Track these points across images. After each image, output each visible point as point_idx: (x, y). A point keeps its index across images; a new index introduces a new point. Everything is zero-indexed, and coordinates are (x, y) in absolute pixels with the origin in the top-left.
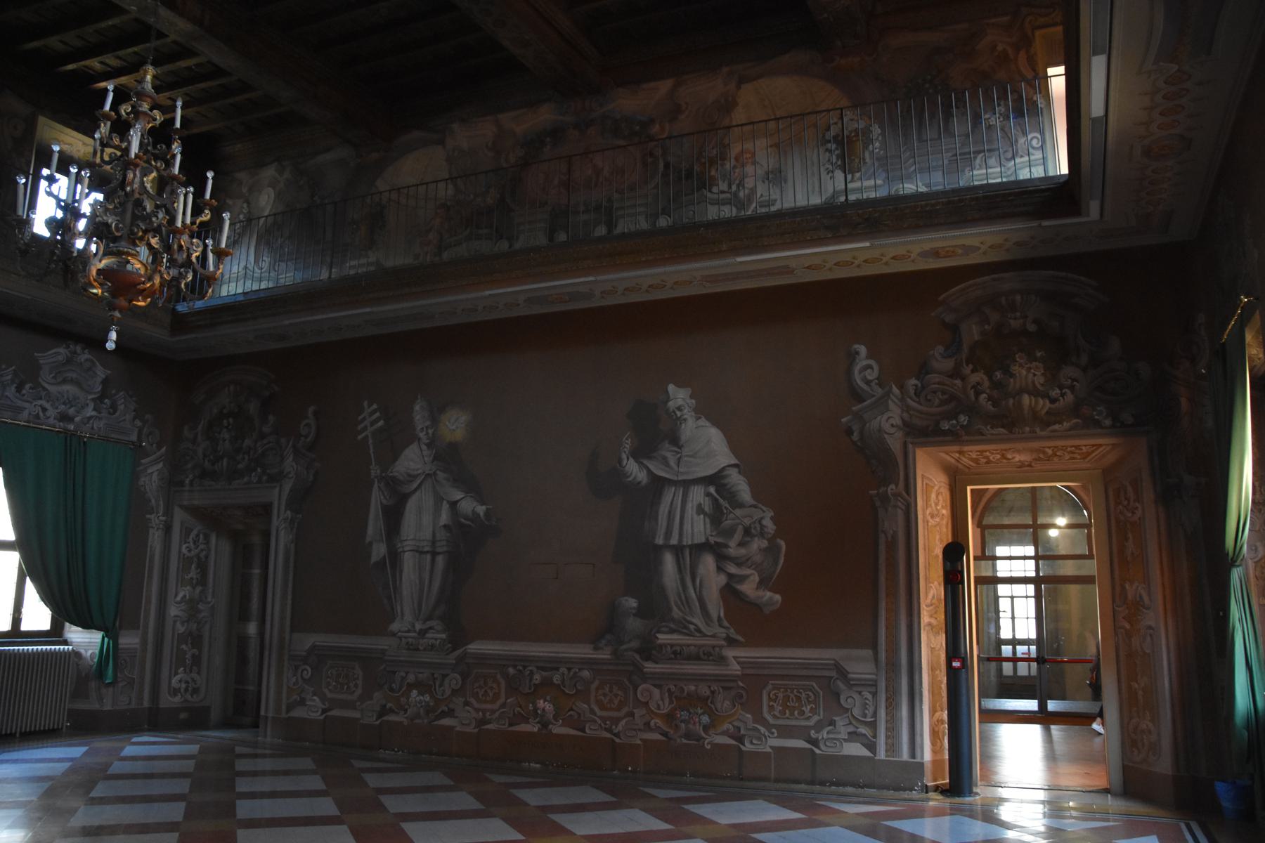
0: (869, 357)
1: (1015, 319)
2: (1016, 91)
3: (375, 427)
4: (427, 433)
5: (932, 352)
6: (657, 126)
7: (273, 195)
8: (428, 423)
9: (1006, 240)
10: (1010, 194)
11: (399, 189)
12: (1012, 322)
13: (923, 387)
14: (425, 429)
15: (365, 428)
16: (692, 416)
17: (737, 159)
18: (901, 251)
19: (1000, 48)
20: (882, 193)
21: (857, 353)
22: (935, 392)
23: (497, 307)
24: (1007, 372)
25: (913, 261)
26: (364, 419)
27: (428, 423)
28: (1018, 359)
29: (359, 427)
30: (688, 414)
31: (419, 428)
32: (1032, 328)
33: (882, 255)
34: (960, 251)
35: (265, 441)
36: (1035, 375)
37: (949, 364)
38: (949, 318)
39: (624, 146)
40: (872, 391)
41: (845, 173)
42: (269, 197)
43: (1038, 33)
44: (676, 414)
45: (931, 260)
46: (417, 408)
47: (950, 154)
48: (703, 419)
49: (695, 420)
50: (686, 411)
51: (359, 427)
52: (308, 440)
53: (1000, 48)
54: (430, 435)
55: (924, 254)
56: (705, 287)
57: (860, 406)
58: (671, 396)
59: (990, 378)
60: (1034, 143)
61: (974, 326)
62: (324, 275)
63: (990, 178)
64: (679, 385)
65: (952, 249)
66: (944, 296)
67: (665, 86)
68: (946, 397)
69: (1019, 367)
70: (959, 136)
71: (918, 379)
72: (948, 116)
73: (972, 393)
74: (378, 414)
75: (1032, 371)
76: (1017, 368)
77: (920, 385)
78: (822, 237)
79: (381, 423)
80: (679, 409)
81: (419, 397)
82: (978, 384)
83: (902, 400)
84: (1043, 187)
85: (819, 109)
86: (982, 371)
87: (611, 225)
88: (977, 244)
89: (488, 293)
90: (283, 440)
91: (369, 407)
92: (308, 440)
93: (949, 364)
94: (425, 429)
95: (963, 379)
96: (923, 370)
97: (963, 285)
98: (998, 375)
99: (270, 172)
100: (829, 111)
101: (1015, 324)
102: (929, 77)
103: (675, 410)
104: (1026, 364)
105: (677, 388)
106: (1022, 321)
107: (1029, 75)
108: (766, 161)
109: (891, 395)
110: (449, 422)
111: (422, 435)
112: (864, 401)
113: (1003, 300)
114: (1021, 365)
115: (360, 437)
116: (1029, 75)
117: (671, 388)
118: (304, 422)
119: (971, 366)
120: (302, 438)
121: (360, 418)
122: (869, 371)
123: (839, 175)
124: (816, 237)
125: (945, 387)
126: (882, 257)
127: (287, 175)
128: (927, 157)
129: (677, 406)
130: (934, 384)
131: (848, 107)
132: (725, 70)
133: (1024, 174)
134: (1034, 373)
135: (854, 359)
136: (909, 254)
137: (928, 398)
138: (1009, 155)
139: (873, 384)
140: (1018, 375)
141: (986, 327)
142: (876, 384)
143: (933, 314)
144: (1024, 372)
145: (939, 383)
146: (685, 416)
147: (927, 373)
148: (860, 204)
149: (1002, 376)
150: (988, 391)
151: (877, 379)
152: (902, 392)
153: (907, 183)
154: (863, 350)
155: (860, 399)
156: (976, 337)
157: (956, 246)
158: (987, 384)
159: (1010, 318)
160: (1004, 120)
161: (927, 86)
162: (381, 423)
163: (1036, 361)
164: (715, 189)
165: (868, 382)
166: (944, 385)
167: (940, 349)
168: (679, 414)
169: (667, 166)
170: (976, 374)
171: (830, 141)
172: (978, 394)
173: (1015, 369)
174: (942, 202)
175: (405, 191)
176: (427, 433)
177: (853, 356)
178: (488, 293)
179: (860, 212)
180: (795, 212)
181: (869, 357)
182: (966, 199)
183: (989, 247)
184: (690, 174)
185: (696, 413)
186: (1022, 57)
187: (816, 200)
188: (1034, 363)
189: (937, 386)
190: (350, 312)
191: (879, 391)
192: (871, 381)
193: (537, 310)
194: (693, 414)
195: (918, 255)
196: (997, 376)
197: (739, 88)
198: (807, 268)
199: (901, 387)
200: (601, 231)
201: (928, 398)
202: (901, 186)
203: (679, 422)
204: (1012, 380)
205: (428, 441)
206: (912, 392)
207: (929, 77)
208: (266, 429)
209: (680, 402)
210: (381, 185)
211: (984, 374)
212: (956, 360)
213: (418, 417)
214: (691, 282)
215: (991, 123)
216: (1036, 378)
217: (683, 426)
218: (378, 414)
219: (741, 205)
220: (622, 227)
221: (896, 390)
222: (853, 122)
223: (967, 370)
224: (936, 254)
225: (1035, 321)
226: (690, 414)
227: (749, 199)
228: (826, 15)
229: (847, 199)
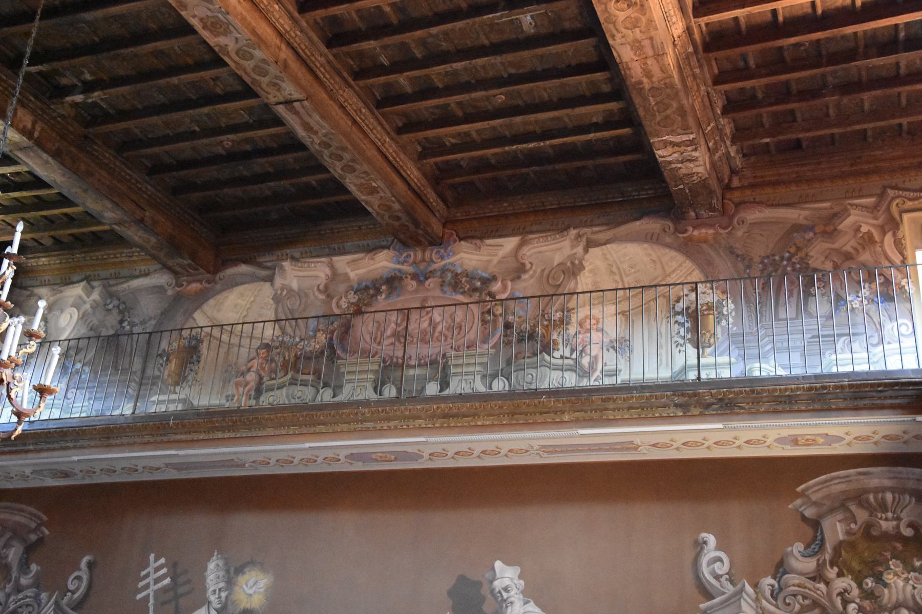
0: (718, 548)
1: (886, 519)
2: (883, 275)
3: (160, 585)
4: (220, 597)
5: (789, 549)
6: (500, 283)
7: (75, 317)
8: (222, 585)
9: (904, 432)
10: (879, 385)
11: (223, 325)
12: (882, 522)
13: (781, 589)
14: (217, 592)
15: (147, 586)
16: (519, 599)
17: (581, 325)
18: (756, 435)
19: (864, 229)
20: (736, 372)
21: (705, 543)
22: (795, 596)
23: (269, 463)
24: (879, 579)
25: (769, 447)
26: (147, 575)
27: (222, 585)
28: (892, 567)
29: (141, 584)
30: (515, 596)
31: (212, 589)
32: (908, 532)
33: (735, 438)
34: (821, 440)
35: (20, 596)
36: (914, 588)
37: (810, 565)
38: (809, 512)
39: (467, 304)
40: (722, 587)
41: (698, 348)
42: (71, 317)
43: (906, 217)
44: (502, 596)
45: (789, 447)
46: (211, 566)
47: (810, 336)
48: (532, 603)
49: (522, 603)
50: (512, 593)
51: (141, 584)
52: (76, 596)
53: (864, 229)
54: (223, 599)
55: (780, 440)
56: (541, 457)
57: (709, 603)
58: (498, 575)
59: (860, 585)
60: (903, 330)
61: (838, 524)
62: (127, 409)
63: (841, 365)
64: (508, 563)
65: (813, 438)
66: (803, 486)
67: (510, 243)
68: (807, 602)
69: (894, 576)
70: (821, 317)
71: (774, 578)
72: (808, 294)
73: (838, 601)
74: (164, 571)
75: (911, 582)
76: (891, 576)
77: (776, 586)
78: (672, 415)
79: (167, 581)
80: (506, 589)
81: (216, 553)
82: (846, 591)
83: (757, 600)
84: (917, 380)
85: (670, 280)
86: (850, 577)
87: (445, 384)
88: (843, 435)
89: (307, 445)
90: (44, 596)
91: (156, 561)
92: (76, 596)
93: (810, 565)
94: (217, 592)
95: (827, 584)
96: (780, 568)
97: (823, 477)
98: (869, 583)
99: (76, 291)
100: (683, 284)
101: (887, 526)
102: (787, 255)
103: (502, 591)
104: (903, 573)
105: (506, 567)
106: (895, 523)
107: (897, 259)
108: (612, 328)
109: (744, 594)
110: (246, 584)
111: (213, 598)
112: (714, 598)
113: (871, 497)
114: (896, 574)
115: (139, 596)
116: (897, 259)
117: (498, 564)
118: (76, 574)
119: (836, 569)
120: (69, 594)
121: (143, 573)
122: (718, 564)
123: (691, 351)
124: (665, 415)
125: (807, 591)
126: (704, 442)
127: (95, 296)
128: (801, 328)
129: (503, 586)
130: (794, 585)
131: (702, 282)
132: (573, 232)
133: (893, 364)
134: (913, 586)
135: (702, 549)
136: (765, 439)
137: (787, 601)
138: (875, 340)
139: (723, 579)
140: (893, 585)
141: (853, 526)
142: (727, 580)
143: (790, 506)
144: (901, 583)
145: (799, 586)
146: (512, 599)
147: (785, 573)
148: (711, 383)
149: (874, 584)
150: (858, 600)
151: (727, 574)
152: (756, 593)
153: (765, 363)
154: (711, 539)
155: (709, 596)
156: (841, 537)
157: (819, 435)
158: (856, 592)
159: (881, 518)
160: (868, 303)
161: (785, 263)
162: (167, 581)
163: (915, 572)
164: (557, 354)
165: (717, 577)
166: (805, 588)
167: (798, 547)
168: (505, 595)
169: (508, 326)
170: (842, 579)
171: (678, 313)
172: (845, 603)
173: (889, 577)
174: (768, 390)
175: (229, 328)
176: (220, 597)
177: (700, 545)
178: (307, 445)
179: (714, 391)
180: (643, 387)
181: (718, 548)
182: (830, 386)
183: (855, 438)
184: (532, 336)
185: (524, 596)
186: (889, 239)
187: (665, 374)
188: (912, 573)
189: (796, 588)
190: (110, 456)
191: (730, 589)
192: (721, 576)
193: (358, 467)
194: (521, 596)
195: (775, 441)
196: (867, 584)
197: (586, 251)
198: (654, 445)
199: (755, 586)
200: (432, 389)
201: (787, 601)
202: (757, 365)
203: (504, 606)
204: (886, 591)
205: (219, 606)
206: (768, 593)
207: (787, 255)
208: (24, 581)
209: (507, 582)
210: (200, 319)
211: (852, 579)
212: (818, 560)
213: (211, 577)
214: (527, 451)
215: (854, 306)
216: (916, 591)
217: (509, 609)
218: (164, 571)
219: (586, 373)
220: (456, 386)
221: (749, 588)
222: (708, 295)
223: (832, 573)
224: (795, 441)
225: (910, 525)
226: (517, 596)
227: (592, 366)
228: (681, 187)
229: (699, 378)
